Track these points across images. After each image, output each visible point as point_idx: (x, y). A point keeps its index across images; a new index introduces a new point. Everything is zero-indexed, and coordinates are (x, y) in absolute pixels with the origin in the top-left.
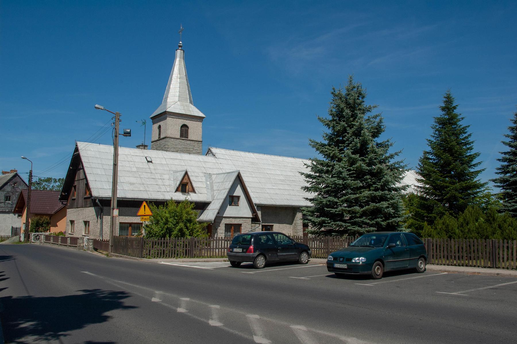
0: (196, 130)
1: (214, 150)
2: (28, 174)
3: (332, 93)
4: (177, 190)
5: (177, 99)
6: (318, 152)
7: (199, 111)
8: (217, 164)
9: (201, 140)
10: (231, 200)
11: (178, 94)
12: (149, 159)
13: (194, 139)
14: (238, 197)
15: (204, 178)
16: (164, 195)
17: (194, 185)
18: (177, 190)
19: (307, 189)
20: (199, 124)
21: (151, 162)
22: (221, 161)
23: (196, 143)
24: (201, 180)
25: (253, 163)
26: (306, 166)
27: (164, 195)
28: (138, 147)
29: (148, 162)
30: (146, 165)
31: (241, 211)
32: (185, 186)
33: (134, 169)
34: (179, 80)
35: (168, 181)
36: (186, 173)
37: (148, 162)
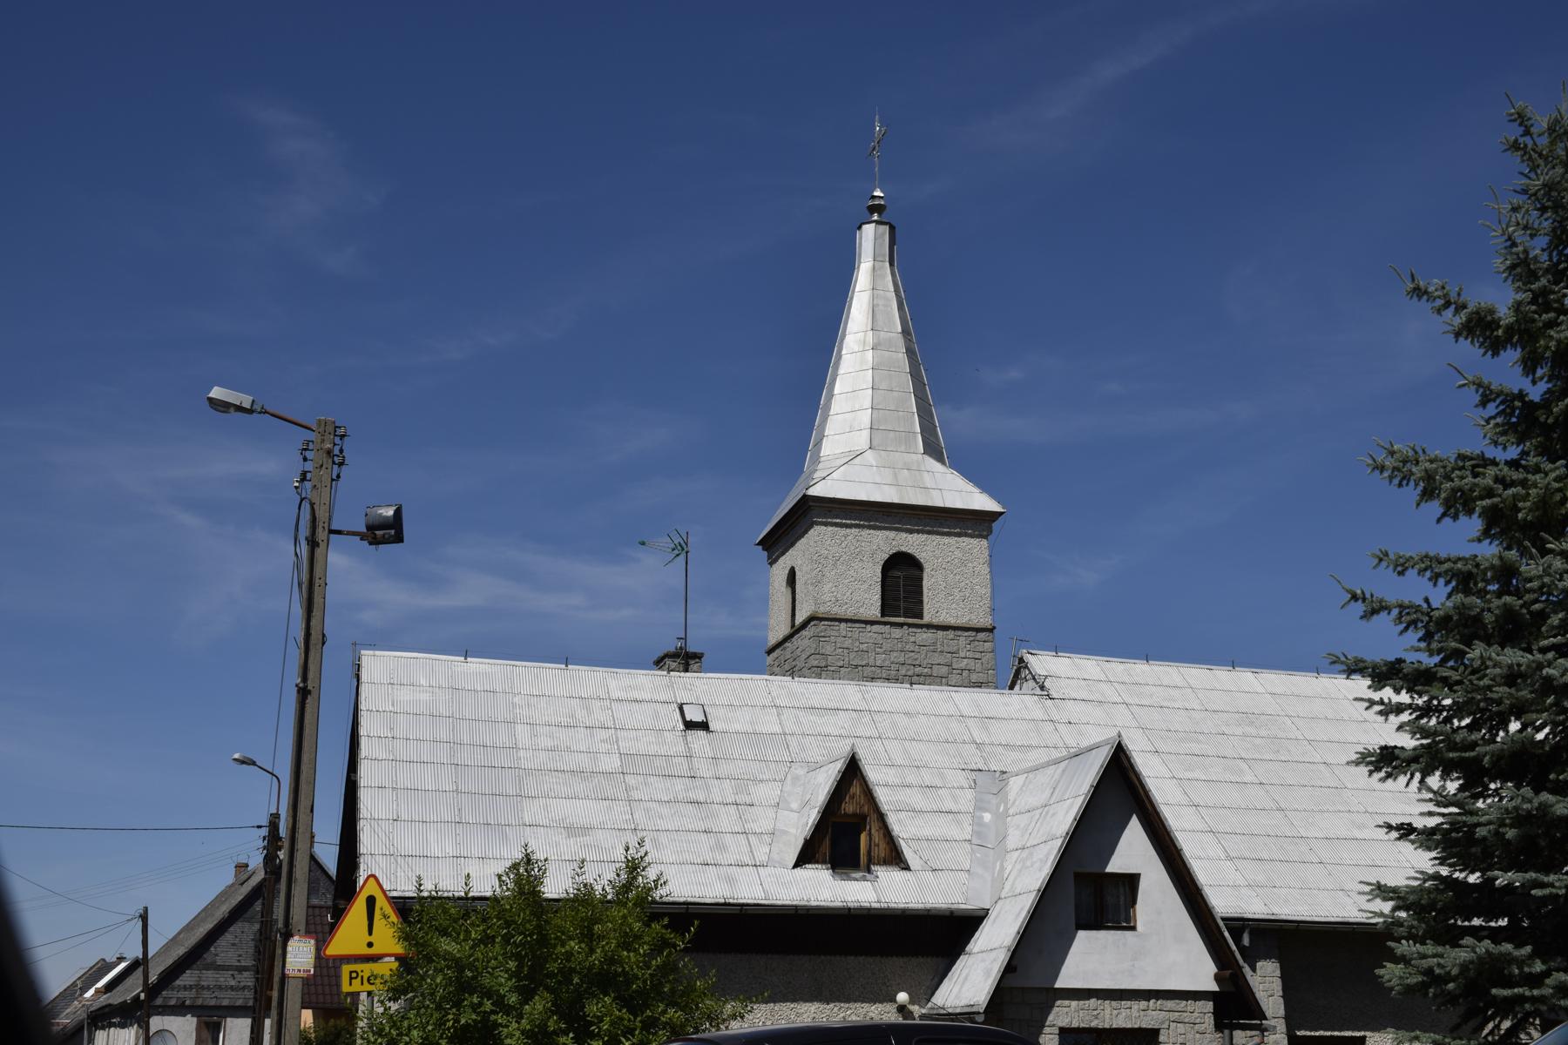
0: (957, 578)
1: (1041, 663)
2: (264, 832)
3: (1515, 146)
4: (806, 857)
5: (862, 440)
6: (1435, 507)
7: (970, 487)
8: (1049, 727)
9: (984, 620)
10: (1085, 892)
11: (865, 418)
12: (694, 715)
13: (952, 621)
14: (1130, 882)
15: (969, 794)
16: (731, 881)
17: (900, 826)
18: (806, 857)
19: (1386, 761)
20: (975, 548)
21: (704, 726)
22: (1073, 710)
23: (963, 639)
24: (949, 805)
25: (1247, 716)
26: (1359, 608)
27: (731, 881)
28: (659, 663)
29: (690, 725)
30: (675, 740)
31: (1156, 953)
32: (848, 828)
33: (612, 763)
34: (870, 354)
35: (771, 813)
36: (853, 770)
37: (690, 725)
